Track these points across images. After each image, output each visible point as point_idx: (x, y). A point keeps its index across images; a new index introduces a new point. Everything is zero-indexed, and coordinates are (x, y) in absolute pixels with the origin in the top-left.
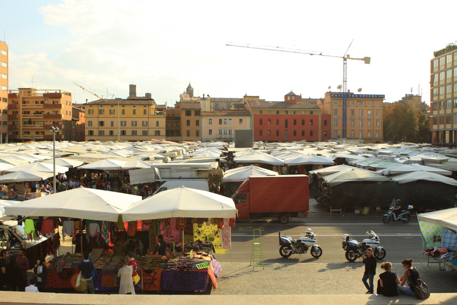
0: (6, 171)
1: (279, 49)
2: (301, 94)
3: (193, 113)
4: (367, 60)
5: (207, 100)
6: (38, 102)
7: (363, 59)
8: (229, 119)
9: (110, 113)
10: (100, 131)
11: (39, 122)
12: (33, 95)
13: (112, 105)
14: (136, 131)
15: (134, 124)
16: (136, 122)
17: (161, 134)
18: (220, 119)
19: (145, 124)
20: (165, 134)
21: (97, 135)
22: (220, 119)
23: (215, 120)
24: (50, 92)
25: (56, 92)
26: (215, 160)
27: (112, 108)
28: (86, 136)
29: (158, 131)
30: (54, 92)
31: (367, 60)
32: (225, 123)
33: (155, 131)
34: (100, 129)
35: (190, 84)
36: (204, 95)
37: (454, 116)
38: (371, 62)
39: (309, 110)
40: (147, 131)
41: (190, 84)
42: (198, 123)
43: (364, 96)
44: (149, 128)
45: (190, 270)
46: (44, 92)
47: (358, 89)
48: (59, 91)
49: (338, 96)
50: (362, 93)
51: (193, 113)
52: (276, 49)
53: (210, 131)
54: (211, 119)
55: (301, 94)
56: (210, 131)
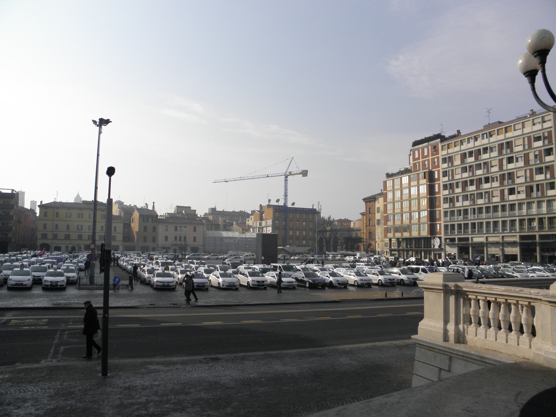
1: (241, 179)
3: (150, 220)
4: (305, 173)
5: (154, 206)
7: (300, 174)
8: (184, 227)
9: (78, 217)
10: (54, 234)
16: (82, 226)
18: (175, 226)
19: (80, 227)
20: (122, 239)
22: (175, 226)
23: (171, 228)
27: (81, 212)
28: (39, 239)
30: (10, 192)
31: (305, 173)
34: (54, 233)
36: (201, 216)
37: (413, 226)
38: (308, 174)
39: (448, 354)
42: (154, 229)
43: (300, 209)
44: (53, 231)
51: (150, 220)
52: (239, 179)
53: (166, 238)
54: (168, 226)
56: (166, 238)
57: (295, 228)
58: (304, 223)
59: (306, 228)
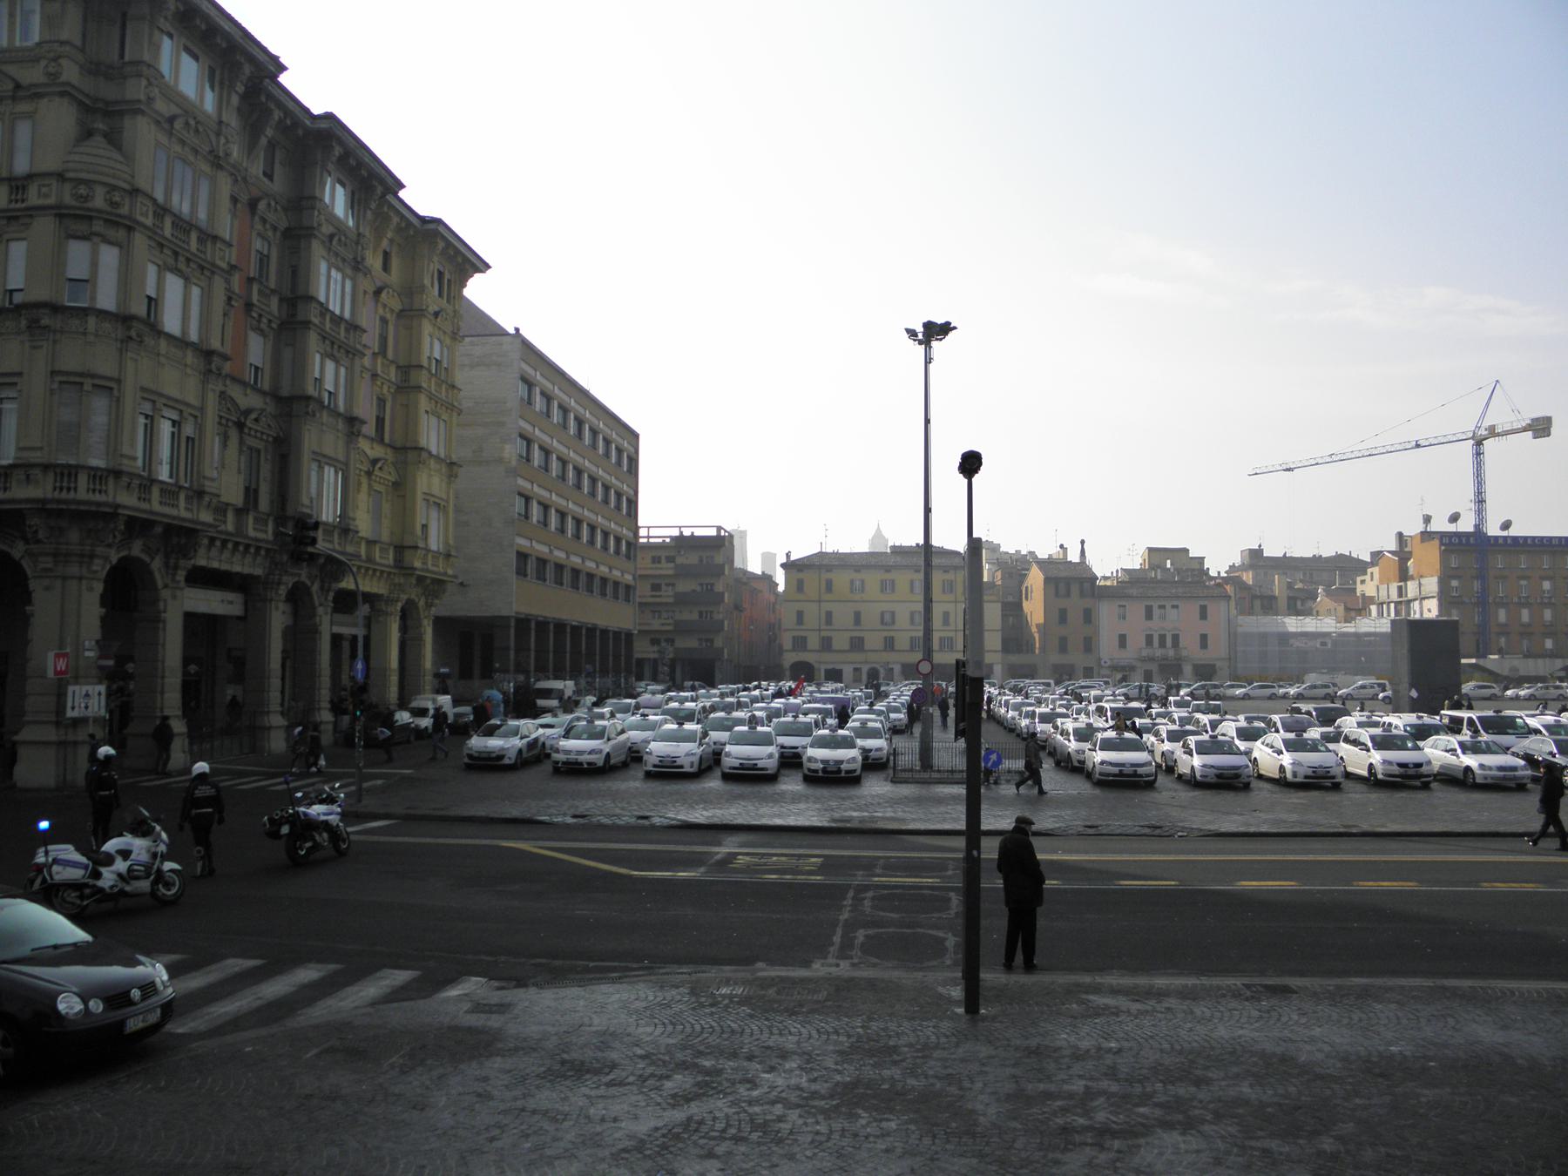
0: (1457, 789)
2: (1260, 546)
3: (1075, 589)
4: (1541, 427)
5: (1083, 552)
6: (660, 558)
7: (1525, 430)
8: (1173, 607)
10: (823, 638)
11: (659, 612)
12: (645, 540)
13: (858, 569)
14: (806, 638)
15: (887, 620)
17: (810, 646)
19: (887, 618)
21: (817, 648)
24: (699, 532)
25: (681, 532)
26: (553, 696)
27: (858, 576)
29: (859, 638)
31: (1541, 427)
32: (1163, 617)
33: (852, 638)
34: (824, 634)
35: (878, 528)
40: (952, 638)
41: (878, 528)
42: (1088, 616)
43: (1509, 541)
45: (837, 939)
46: (675, 533)
47: (1503, 524)
48: (715, 529)
49: (1460, 540)
50: (1513, 532)
51: (1075, 589)
53: (1122, 641)
55: (1260, 546)
56: (1122, 641)
57: (1516, 600)
58: (1547, 585)
59: (1553, 600)
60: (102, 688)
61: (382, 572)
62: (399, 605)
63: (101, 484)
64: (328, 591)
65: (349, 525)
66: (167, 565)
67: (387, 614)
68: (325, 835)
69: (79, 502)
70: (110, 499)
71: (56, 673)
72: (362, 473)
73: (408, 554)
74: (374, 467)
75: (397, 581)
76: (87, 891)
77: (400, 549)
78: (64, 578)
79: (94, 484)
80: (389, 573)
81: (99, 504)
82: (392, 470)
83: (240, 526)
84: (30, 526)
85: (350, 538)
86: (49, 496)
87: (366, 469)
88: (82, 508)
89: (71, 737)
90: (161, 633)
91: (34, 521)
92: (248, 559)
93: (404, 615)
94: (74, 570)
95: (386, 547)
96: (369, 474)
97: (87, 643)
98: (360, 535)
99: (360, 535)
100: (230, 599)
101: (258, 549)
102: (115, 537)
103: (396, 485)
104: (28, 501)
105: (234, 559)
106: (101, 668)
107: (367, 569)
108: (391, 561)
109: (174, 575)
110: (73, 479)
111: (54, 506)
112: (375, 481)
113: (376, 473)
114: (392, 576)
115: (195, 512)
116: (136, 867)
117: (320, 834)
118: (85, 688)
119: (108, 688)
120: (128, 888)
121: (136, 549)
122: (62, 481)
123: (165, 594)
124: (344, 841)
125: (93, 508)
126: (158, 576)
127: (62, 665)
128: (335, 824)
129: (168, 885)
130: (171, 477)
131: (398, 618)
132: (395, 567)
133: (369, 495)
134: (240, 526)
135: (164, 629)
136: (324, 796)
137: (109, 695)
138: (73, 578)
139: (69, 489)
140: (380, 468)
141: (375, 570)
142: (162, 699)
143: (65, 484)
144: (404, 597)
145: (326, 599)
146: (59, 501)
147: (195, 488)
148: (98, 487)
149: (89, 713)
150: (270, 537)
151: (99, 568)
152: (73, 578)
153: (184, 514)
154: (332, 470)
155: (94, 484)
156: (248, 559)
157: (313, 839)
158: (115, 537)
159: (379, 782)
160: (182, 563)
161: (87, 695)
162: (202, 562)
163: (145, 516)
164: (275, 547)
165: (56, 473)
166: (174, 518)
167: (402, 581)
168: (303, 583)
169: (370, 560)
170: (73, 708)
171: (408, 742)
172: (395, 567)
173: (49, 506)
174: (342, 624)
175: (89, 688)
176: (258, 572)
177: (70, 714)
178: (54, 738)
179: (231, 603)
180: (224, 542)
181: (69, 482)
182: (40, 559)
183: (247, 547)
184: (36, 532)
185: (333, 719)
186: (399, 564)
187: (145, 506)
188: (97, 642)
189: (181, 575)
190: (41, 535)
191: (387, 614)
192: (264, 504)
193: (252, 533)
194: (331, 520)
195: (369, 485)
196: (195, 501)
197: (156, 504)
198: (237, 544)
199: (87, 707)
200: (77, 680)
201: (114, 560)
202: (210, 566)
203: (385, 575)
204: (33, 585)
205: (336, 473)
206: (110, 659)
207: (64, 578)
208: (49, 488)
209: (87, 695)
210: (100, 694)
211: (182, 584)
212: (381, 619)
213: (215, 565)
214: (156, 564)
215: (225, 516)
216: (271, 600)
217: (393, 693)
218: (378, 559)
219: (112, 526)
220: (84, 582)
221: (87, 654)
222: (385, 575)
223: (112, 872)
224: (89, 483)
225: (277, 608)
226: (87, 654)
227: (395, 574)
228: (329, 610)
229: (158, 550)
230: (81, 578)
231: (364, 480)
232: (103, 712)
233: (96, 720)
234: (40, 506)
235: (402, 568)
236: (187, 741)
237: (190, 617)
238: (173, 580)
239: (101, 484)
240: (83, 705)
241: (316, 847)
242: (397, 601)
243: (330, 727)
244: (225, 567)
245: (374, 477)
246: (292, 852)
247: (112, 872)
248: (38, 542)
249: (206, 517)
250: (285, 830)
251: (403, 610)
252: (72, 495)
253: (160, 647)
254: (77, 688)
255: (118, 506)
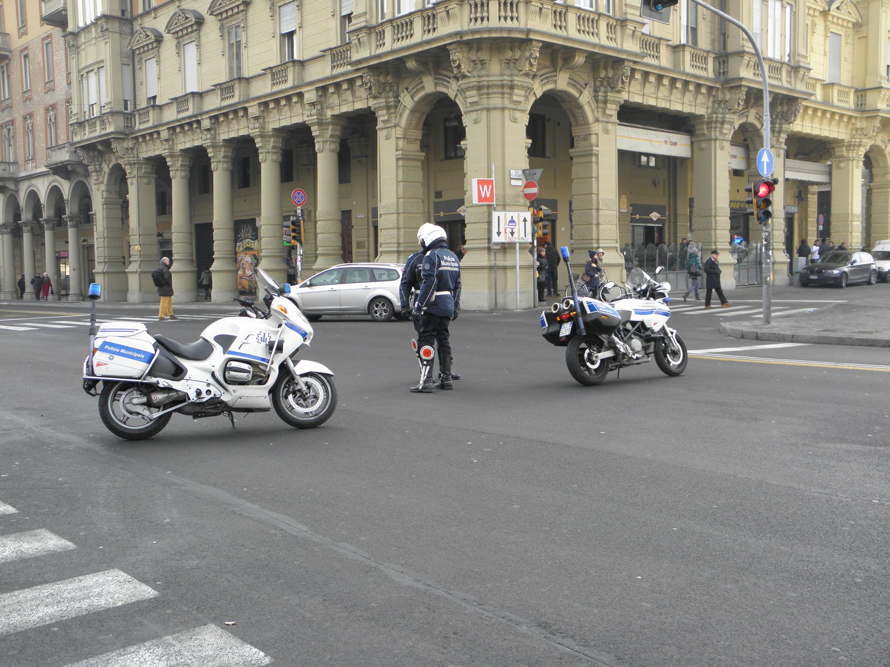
60: (528, 215)
61: (842, 116)
62: (862, 151)
63: (512, 11)
64: (780, 132)
65: (799, 62)
66: (596, 97)
67: (848, 159)
68: (637, 343)
69: (490, 30)
70: (522, 26)
71: (480, 199)
72: (817, 14)
73: (870, 96)
74: (830, 6)
75: (859, 125)
76: (157, 397)
77: (861, 93)
78: (488, 110)
79: (505, 11)
80: (850, 117)
81: (510, 30)
82: (852, 9)
83: (676, 63)
84: (454, 61)
85: (800, 76)
86: (466, 28)
87: (821, 9)
88: (494, 35)
89: (500, 263)
90: (594, 166)
91: (456, 56)
92: (689, 97)
93: (868, 162)
94: (496, 101)
95: (846, 90)
96: (825, 14)
97: (513, 172)
98: (812, 74)
99: (812, 74)
100: (674, 140)
101: (698, 86)
102: (531, 65)
103: (857, 26)
104: (450, 36)
105: (673, 98)
106: (527, 196)
107: (824, 112)
108: (852, 105)
109: (605, 109)
110: (485, 8)
111: (470, 37)
112: (833, 23)
113: (831, 12)
114: (853, 121)
115: (619, 41)
116: (234, 364)
117: (627, 341)
118: (509, 215)
119: (534, 215)
120: (226, 398)
121: (562, 82)
122: (476, 12)
123: (596, 128)
124: (675, 354)
125: (505, 35)
126: (587, 109)
127: (486, 192)
128: (656, 328)
129: (303, 397)
130: (591, 6)
131: (861, 164)
132: (855, 110)
133: (826, 37)
134: (676, 63)
135: (597, 163)
136: (644, 287)
137: (535, 222)
138: (495, 109)
139: (482, 19)
140: (838, 8)
141: (833, 114)
142: (598, 230)
143: (479, 15)
144: (868, 143)
145: (778, 141)
146: (474, 32)
147: (618, 16)
148: (509, 14)
149: (516, 239)
150: (711, 75)
151: (521, 99)
152: (495, 109)
153: (604, 41)
154: (778, 4)
155: (505, 11)
156: (689, 97)
157: (612, 346)
158: (531, 65)
159: (811, 310)
160: (611, 95)
161: (512, 221)
162: (637, 99)
163: (560, 42)
164: (718, 86)
165: (471, 5)
166: (594, 45)
167: (864, 124)
168: (752, 125)
169: (826, 102)
170: (499, 233)
171: (869, 283)
172: (855, 110)
173: (466, 38)
174: (792, 169)
175: (515, 215)
176: (700, 111)
177: (495, 239)
178: (485, 263)
179: (675, 144)
180: (660, 78)
181: (482, 12)
182: (468, 94)
183: (686, 83)
184: (459, 66)
185: (789, 260)
186: (861, 107)
187: (563, 33)
188: (524, 171)
189: (613, 110)
190: (464, 69)
191: (848, 159)
192: (704, 41)
193: (689, 69)
194: (778, 57)
195: (826, 26)
196: (618, 28)
197: (572, 30)
198: (673, 81)
199: (512, 233)
200: (504, 207)
201: (539, 94)
202: (645, 103)
203: (845, 119)
204: (466, 120)
205: (783, 7)
206: (535, 186)
207: (488, 110)
208: (466, 19)
209: (512, 221)
210: (525, 220)
211: (615, 118)
212: (842, 165)
213: (652, 102)
214: (585, 98)
215: (658, 51)
216: (716, 140)
217: (856, 237)
218: (836, 102)
219: (528, 54)
220: (507, 112)
221: (514, 182)
222: (845, 119)
223: (205, 370)
224: (500, 10)
225: (722, 148)
226: (514, 182)
227: (856, 117)
228: (782, 152)
229: (586, 84)
230: (503, 109)
231: (820, 22)
232: (529, 239)
233: (523, 246)
234: (458, 39)
235: (863, 111)
236: (625, 271)
237: (623, 155)
238: (604, 113)
239: (512, 11)
240: (509, 231)
241: (618, 360)
242: (859, 146)
243: (785, 268)
244: (662, 104)
245: (830, 18)
246: (576, 364)
247: (205, 370)
248: (464, 77)
249: (632, 46)
250: (566, 330)
251: (866, 156)
252: (485, 24)
253: (594, 180)
254: (501, 214)
255: (529, 31)
